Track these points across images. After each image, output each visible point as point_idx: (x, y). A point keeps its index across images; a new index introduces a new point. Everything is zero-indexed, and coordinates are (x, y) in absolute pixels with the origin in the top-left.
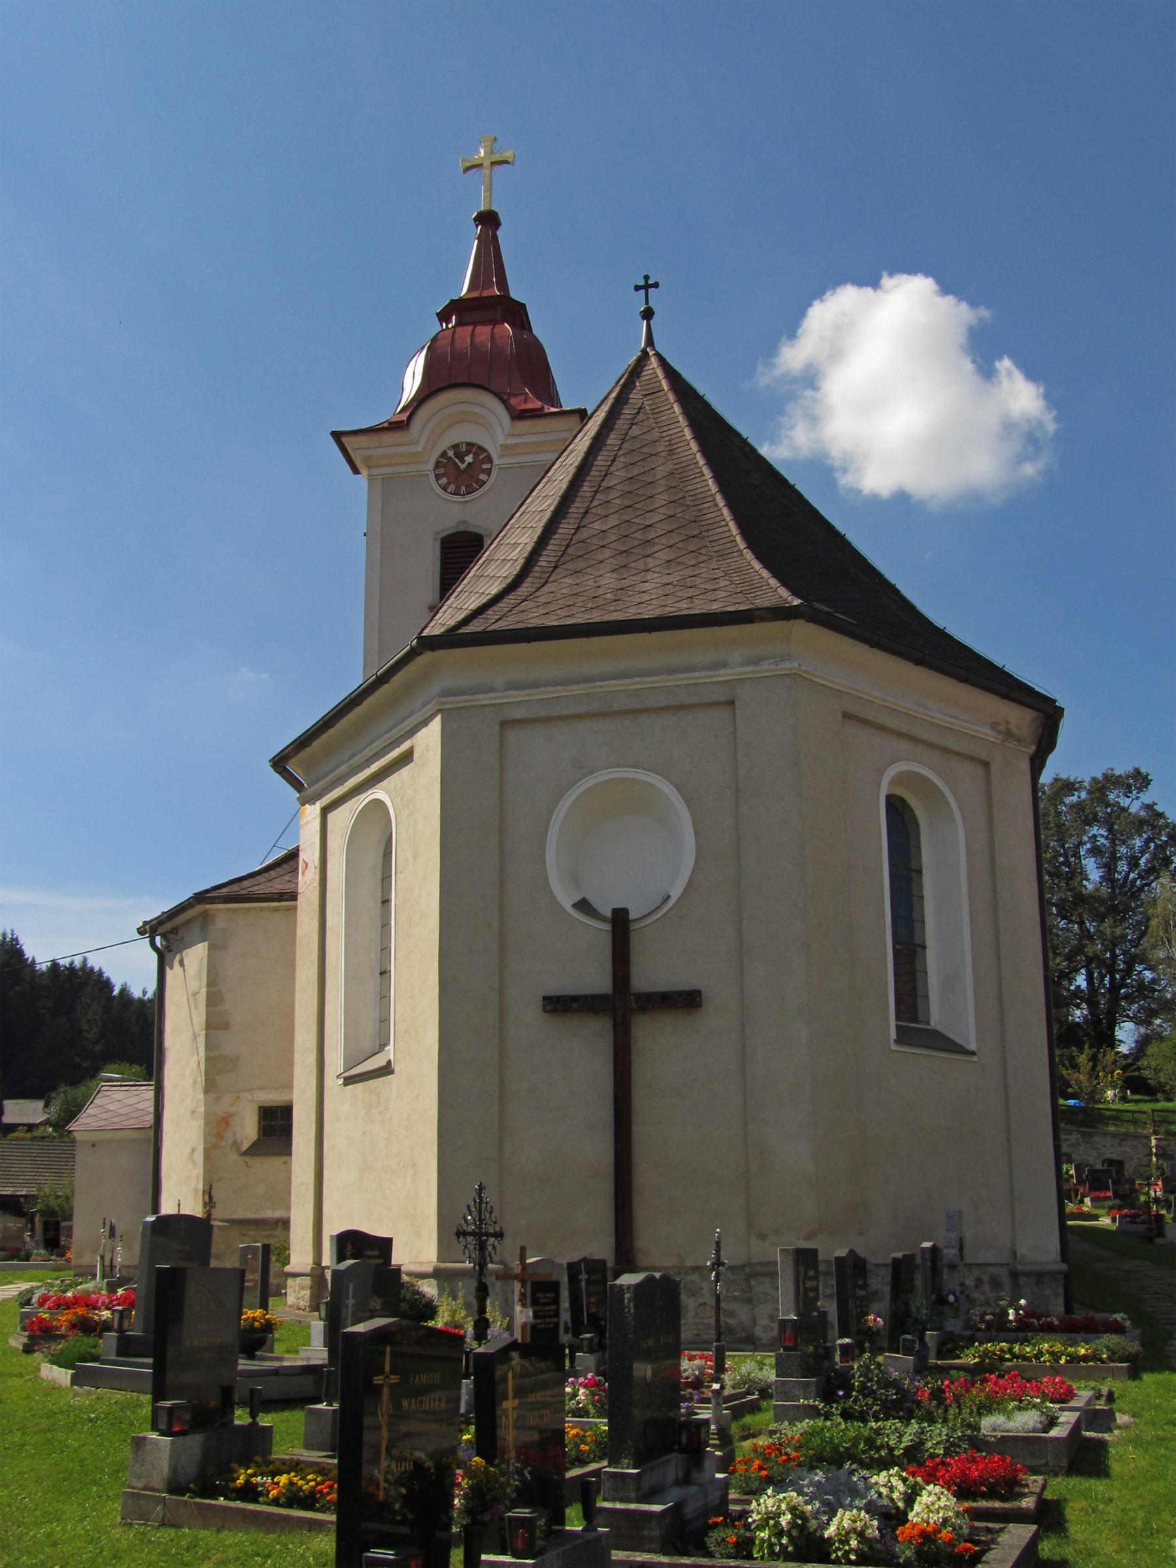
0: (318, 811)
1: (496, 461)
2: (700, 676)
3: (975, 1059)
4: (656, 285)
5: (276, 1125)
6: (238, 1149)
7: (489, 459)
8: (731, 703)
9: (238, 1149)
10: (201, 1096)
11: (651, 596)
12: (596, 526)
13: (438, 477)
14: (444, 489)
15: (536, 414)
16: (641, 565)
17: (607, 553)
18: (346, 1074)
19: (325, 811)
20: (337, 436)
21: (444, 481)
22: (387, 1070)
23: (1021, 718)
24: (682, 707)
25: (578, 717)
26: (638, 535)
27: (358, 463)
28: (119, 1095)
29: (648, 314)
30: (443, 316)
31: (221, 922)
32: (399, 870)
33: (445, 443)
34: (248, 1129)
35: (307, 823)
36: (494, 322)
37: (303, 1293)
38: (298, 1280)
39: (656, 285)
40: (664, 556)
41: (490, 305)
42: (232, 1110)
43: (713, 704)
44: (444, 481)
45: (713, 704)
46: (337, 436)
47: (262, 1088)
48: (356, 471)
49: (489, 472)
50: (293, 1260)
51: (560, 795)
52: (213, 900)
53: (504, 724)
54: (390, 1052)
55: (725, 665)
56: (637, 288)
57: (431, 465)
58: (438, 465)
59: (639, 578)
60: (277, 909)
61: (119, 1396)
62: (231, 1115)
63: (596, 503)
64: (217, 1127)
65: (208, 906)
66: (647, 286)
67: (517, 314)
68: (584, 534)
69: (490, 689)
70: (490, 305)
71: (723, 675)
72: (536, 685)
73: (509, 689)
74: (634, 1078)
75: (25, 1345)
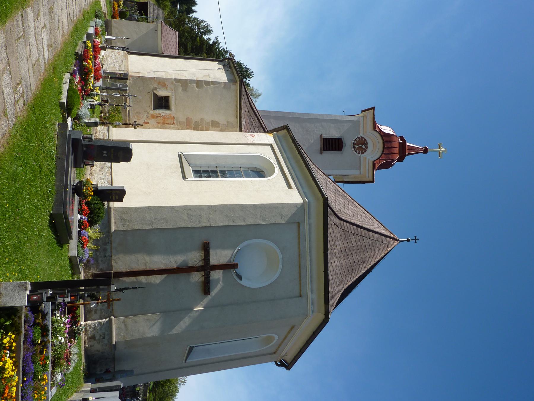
0: (271, 143)
1: (362, 155)
2: (309, 286)
3: (184, 362)
4: (416, 242)
5: (162, 103)
6: (154, 89)
7: (363, 153)
8: (301, 296)
9: (154, 89)
10: (173, 78)
11: (334, 264)
12: (354, 239)
13: (359, 138)
14: (356, 140)
15: (374, 165)
16: (342, 257)
17: (345, 245)
18: (182, 156)
19: (271, 145)
20: (373, 108)
21: (358, 140)
22: (184, 177)
23: (289, 358)
24: (300, 280)
25: (299, 248)
26: (350, 253)
27: (365, 113)
28: (173, 39)
29: (408, 240)
30: (402, 138)
31: (233, 87)
32: (252, 181)
33: (369, 141)
34: (162, 93)
35: (267, 137)
36: (399, 154)
37: (102, 135)
38: (106, 132)
39: (416, 242)
40: (344, 264)
41: (404, 151)
42: (168, 88)
43: (300, 290)
44: (358, 140)
45: (300, 290)
46: (373, 108)
47: (176, 99)
48: (363, 111)
49: (359, 153)
50: (114, 129)
51: (275, 243)
52: (240, 86)
53: (299, 224)
54: (191, 178)
55: (312, 293)
56: (415, 237)
57: (363, 136)
58: (362, 138)
59: (338, 258)
60: (236, 107)
61: (54, 150)
62: (167, 87)
63: (360, 237)
64: (162, 82)
65: (238, 83)
66: (416, 240)
67: (401, 159)
68: (351, 236)
69: (309, 218)
70: (404, 151)
71: (309, 293)
72: (310, 233)
73: (309, 225)
74: (182, 274)
75: (78, 53)
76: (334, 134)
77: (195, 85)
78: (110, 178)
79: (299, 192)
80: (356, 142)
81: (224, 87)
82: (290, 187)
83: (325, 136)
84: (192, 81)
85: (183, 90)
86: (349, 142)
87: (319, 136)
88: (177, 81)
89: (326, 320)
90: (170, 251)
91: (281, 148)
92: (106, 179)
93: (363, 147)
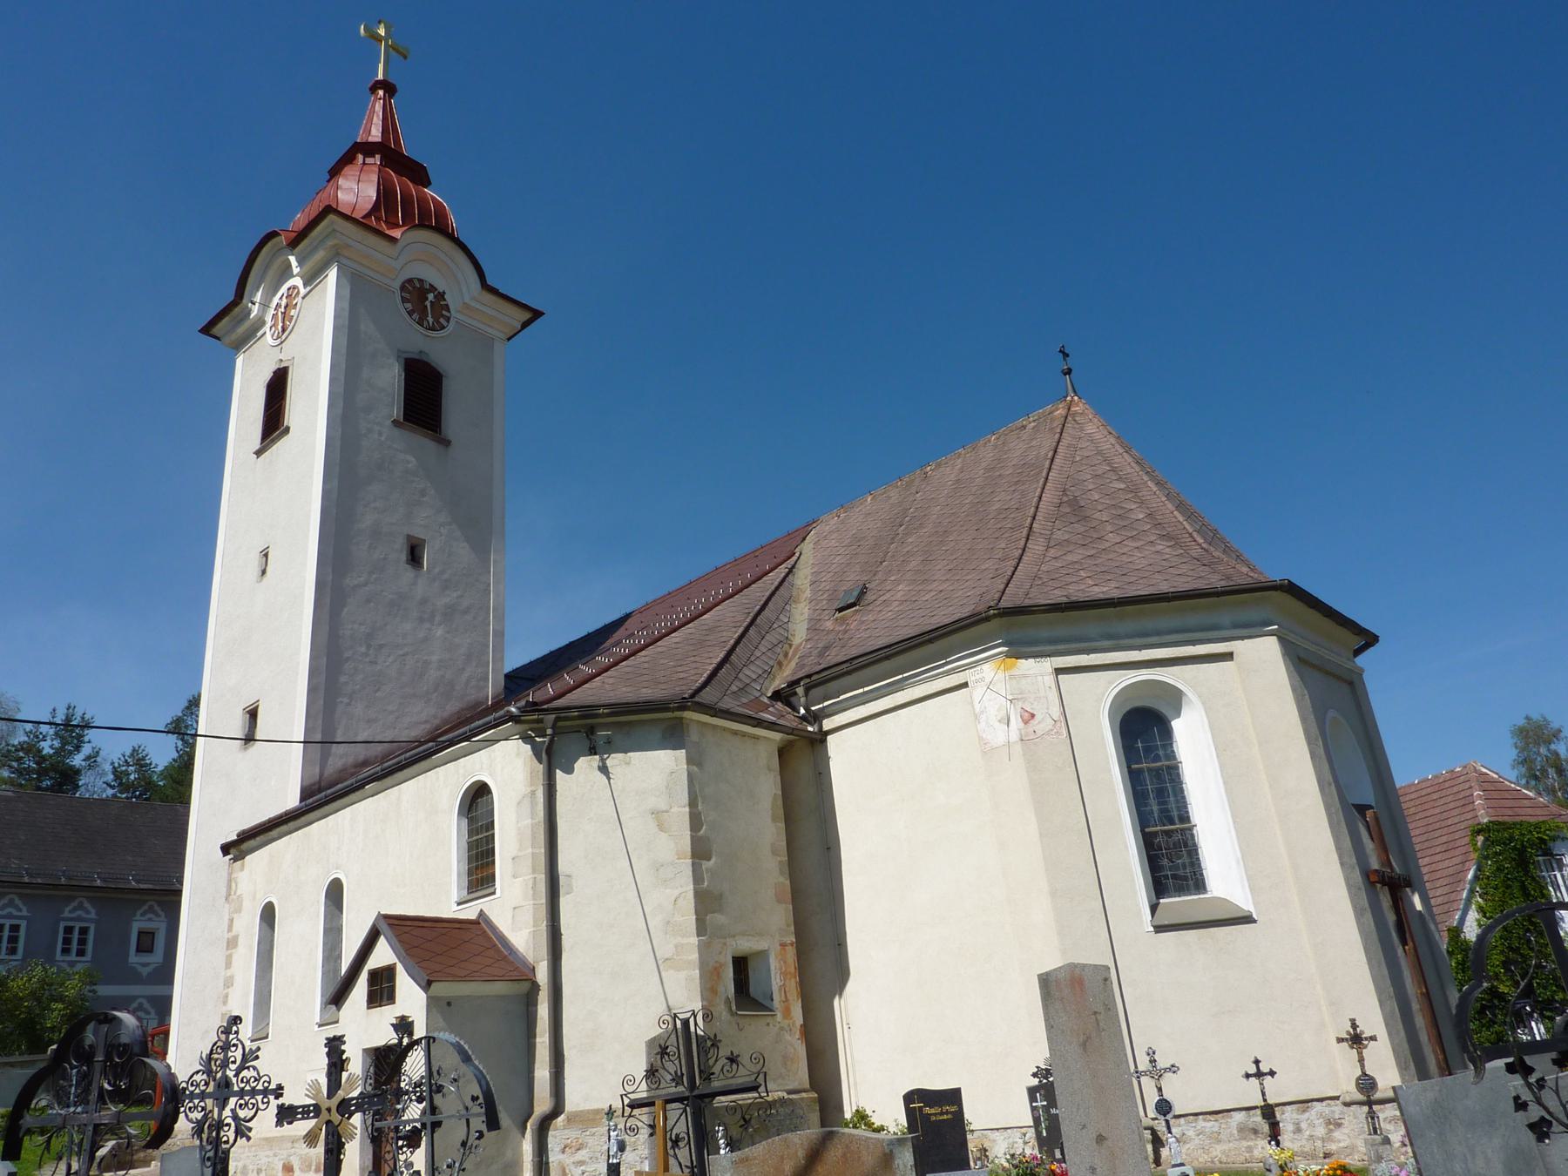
20: (537, 314)
31: (694, 735)
46: (537, 314)
76: (391, 378)
77: (706, 865)
78: (1288, 1108)
79: (1242, 638)
80: (415, 316)
81: (700, 765)
82: (1228, 656)
83: (397, 411)
84: (697, 878)
85: (720, 911)
86: (418, 340)
87: (397, 432)
88: (701, 928)
89: (1291, 589)
90: (1394, 950)
91: (1061, 647)
92: (1295, 1116)
93: (431, 296)
